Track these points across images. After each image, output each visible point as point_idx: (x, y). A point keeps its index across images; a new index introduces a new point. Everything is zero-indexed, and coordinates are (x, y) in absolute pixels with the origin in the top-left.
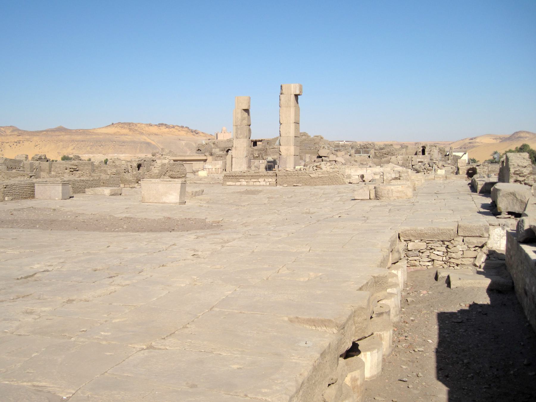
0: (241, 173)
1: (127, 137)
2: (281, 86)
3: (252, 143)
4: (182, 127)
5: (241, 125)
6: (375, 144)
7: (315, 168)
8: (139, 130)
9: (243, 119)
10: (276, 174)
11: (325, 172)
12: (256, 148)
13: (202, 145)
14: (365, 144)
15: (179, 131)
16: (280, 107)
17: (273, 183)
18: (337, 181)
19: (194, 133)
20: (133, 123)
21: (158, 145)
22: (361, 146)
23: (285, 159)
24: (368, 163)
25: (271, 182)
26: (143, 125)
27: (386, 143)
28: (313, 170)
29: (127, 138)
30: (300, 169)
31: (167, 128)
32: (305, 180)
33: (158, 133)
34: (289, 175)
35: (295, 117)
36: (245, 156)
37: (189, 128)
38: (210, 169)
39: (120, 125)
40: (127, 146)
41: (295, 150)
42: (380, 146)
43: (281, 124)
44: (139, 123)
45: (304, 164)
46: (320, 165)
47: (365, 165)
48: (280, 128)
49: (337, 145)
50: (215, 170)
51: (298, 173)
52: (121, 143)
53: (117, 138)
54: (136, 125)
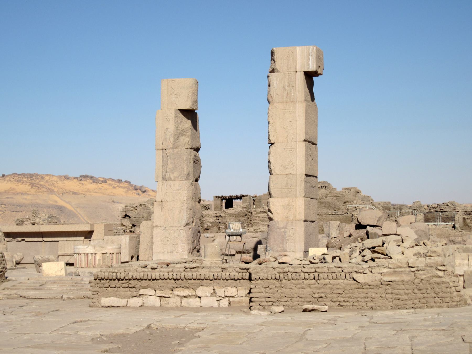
0: (146, 269)
1: (25, 197)
2: (272, 53)
3: (224, 201)
4: (120, 181)
5: (176, 148)
6: (456, 204)
7: (369, 255)
8: (47, 186)
9: (179, 135)
10: (250, 274)
11: (401, 267)
12: (230, 210)
13: (133, 207)
15: (114, 187)
16: (269, 103)
17: (239, 302)
18: (441, 295)
19: (139, 191)
20: (37, 175)
21: (77, 211)
22: (429, 208)
23: (283, 230)
24: (465, 239)
25: (233, 297)
26: (55, 178)
28: (363, 261)
29: (26, 199)
30: (324, 259)
31: (94, 182)
32: (340, 291)
33: (78, 190)
34: (290, 278)
35: (306, 127)
36: (184, 222)
37: (130, 183)
38: (90, 255)
39: (15, 178)
40: (24, 212)
41: (307, 207)
42: (466, 208)
43: (272, 144)
44: (47, 175)
45: (326, 243)
46: (384, 244)
47: (459, 243)
48: (269, 155)
49: (386, 205)
50: (104, 259)
51: (317, 270)
52: (15, 206)
53: (8, 200)
54: (42, 178)
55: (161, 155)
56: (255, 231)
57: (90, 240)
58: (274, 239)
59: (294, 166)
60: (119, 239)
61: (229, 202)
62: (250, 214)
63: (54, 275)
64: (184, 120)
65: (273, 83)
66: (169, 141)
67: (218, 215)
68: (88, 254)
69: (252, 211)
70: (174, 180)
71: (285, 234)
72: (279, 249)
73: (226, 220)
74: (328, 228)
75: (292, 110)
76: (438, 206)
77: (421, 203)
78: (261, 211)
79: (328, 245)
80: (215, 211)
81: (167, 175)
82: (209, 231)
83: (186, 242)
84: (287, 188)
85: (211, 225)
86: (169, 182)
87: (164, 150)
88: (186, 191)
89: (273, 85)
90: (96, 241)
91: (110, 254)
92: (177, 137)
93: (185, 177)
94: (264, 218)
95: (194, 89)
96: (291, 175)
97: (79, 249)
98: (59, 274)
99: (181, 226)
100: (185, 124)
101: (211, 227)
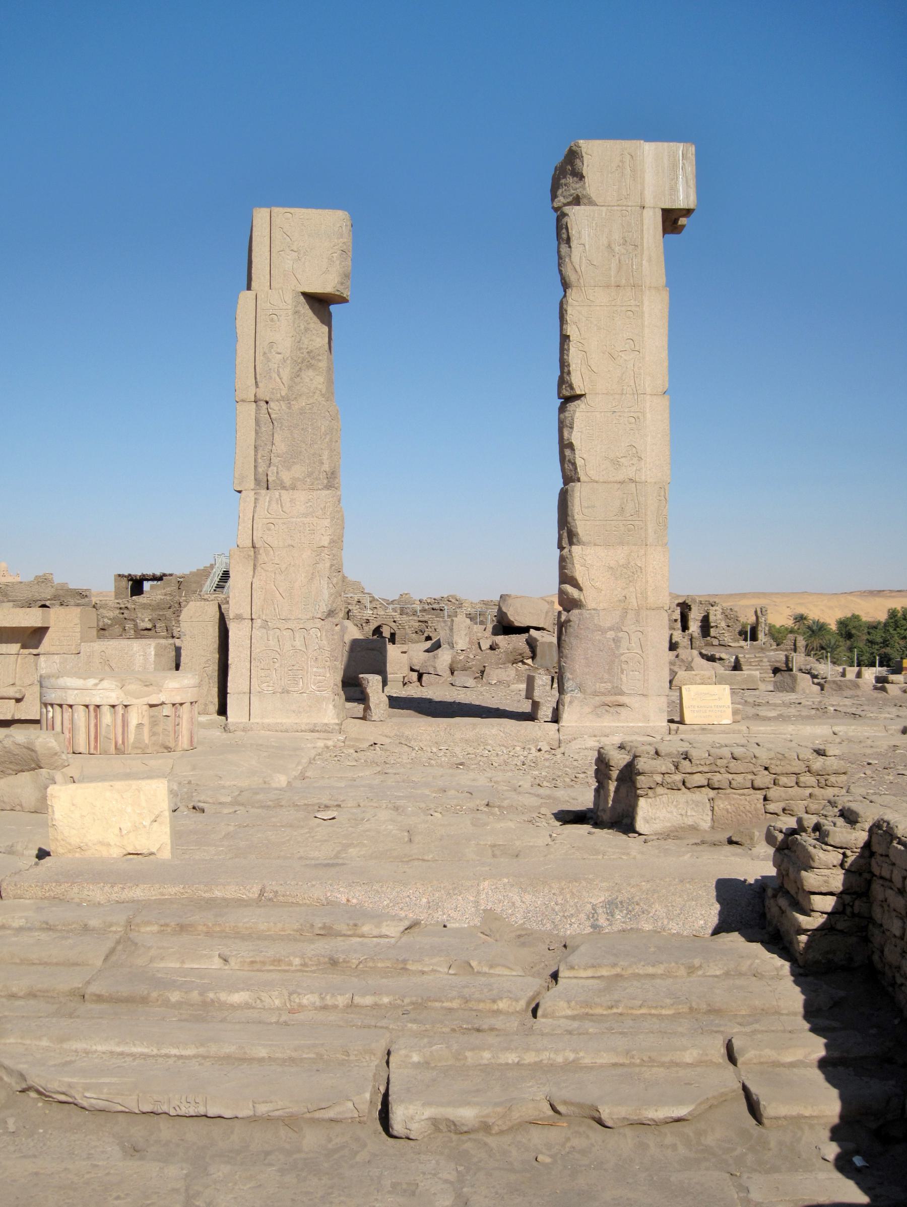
3: (130, 583)
14: (434, 599)
23: (611, 634)
36: (324, 608)
38: (105, 710)
45: (449, 661)
50: (154, 723)
57: (38, 655)
58: (587, 659)
59: (640, 458)
60: (126, 653)
61: (136, 585)
62: (176, 605)
63: (116, 852)
64: (312, 325)
66: (278, 379)
67: (123, 606)
68: (98, 706)
69: (181, 601)
71: (618, 647)
72: (601, 687)
73: (137, 614)
74: (448, 631)
75: (633, 309)
79: (454, 666)
80: (117, 599)
81: (270, 474)
82: (106, 633)
84: (620, 518)
85: (110, 622)
86: (277, 493)
87: (263, 404)
88: (329, 520)
90: (56, 656)
91: (174, 705)
95: (345, 240)
96: (634, 485)
97: (64, 688)
98: (142, 843)
99: (313, 618)
100: (314, 337)
101: (111, 625)
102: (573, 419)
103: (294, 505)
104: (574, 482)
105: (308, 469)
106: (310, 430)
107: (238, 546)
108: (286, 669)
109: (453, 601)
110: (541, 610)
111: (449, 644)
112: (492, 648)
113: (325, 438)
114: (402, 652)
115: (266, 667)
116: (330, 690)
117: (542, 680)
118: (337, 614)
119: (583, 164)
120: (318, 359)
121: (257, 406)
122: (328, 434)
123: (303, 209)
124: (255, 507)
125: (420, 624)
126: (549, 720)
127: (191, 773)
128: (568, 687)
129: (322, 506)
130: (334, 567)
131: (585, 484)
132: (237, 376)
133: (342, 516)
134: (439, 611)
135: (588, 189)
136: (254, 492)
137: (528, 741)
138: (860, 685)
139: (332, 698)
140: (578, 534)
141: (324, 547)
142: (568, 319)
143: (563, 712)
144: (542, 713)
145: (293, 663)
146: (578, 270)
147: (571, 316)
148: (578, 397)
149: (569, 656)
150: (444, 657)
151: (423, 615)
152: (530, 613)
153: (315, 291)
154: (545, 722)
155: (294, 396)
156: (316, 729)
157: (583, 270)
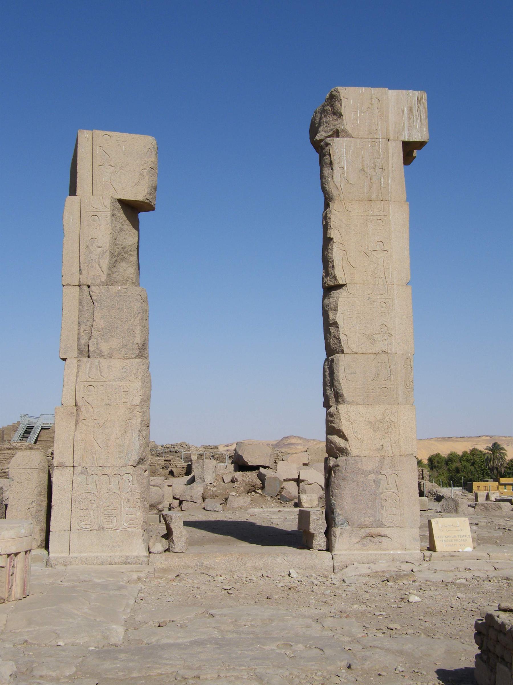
14: (171, 445)
27: (206, 444)
36: (135, 457)
45: (202, 492)
55: (77, 298)
56: (3, 471)
58: (353, 497)
64: (126, 227)
65: (340, 158)
66: (98, 267)
70: (110, 357)
71: (378, 487)
74: (200, 470)
75: (382, 218)
76: (172, 446)
77: (156, 443)
78: (7, 447)
81: (90, 345)
83: (139, 504)
86: (96, 361)
87: (86, 288)
88: (140, 384)
89: (340, 162)
91: (9, 555)
92: (114, 260)
93: (138, 352)
94: (10, 456)
96: (386, 356)
99: (126, 465)
102: (337, 304)
103: (111, 371)
104: (339, 353)
105: (123, 341)
106: (125, 310)
107: (62, 404)
108: (102, 509)
109: (184, 446)
110: (267, 454)
111: (201, 479)
112: (233, 481)
113: (137, 316)
114: (169, 486)
115: (85, 508)
116: (140, 526)
117: (316, 515)
118: (145, 461)
119: (341, 105)
120: (130, 254)
121: (80, 289)
122: (139, 313)
123: (119, 133)
124: (78, 372)
125: (165, 462)
126: (325, 549)
127: (27, 630)
128: (338, 522)
129: (134, 372)
130: (144, 422)
131: (348, 355)
132: (63, 264)
133: (151, 380)
134: (174, 453)
135: (345, 124)
136: (77, 359)
137: (308, 568)
138: (502, 507)
139: (142, 533)
140: (343, 395)
141: (136, 405)
142: (332, 225)
143: (335, 542)
144: (317, 543)
145: (109, 504)
146: (340, 188)
147: (334, 223)
148: (340, 286)
149: (338, 495)
150: (198, 489)
151: (167, 456)
152: (259, 456)
153: (129, 199)
154: (319, 550)
155: (111, 282)
156: (128, 561)
157: (342, 188)
